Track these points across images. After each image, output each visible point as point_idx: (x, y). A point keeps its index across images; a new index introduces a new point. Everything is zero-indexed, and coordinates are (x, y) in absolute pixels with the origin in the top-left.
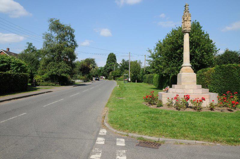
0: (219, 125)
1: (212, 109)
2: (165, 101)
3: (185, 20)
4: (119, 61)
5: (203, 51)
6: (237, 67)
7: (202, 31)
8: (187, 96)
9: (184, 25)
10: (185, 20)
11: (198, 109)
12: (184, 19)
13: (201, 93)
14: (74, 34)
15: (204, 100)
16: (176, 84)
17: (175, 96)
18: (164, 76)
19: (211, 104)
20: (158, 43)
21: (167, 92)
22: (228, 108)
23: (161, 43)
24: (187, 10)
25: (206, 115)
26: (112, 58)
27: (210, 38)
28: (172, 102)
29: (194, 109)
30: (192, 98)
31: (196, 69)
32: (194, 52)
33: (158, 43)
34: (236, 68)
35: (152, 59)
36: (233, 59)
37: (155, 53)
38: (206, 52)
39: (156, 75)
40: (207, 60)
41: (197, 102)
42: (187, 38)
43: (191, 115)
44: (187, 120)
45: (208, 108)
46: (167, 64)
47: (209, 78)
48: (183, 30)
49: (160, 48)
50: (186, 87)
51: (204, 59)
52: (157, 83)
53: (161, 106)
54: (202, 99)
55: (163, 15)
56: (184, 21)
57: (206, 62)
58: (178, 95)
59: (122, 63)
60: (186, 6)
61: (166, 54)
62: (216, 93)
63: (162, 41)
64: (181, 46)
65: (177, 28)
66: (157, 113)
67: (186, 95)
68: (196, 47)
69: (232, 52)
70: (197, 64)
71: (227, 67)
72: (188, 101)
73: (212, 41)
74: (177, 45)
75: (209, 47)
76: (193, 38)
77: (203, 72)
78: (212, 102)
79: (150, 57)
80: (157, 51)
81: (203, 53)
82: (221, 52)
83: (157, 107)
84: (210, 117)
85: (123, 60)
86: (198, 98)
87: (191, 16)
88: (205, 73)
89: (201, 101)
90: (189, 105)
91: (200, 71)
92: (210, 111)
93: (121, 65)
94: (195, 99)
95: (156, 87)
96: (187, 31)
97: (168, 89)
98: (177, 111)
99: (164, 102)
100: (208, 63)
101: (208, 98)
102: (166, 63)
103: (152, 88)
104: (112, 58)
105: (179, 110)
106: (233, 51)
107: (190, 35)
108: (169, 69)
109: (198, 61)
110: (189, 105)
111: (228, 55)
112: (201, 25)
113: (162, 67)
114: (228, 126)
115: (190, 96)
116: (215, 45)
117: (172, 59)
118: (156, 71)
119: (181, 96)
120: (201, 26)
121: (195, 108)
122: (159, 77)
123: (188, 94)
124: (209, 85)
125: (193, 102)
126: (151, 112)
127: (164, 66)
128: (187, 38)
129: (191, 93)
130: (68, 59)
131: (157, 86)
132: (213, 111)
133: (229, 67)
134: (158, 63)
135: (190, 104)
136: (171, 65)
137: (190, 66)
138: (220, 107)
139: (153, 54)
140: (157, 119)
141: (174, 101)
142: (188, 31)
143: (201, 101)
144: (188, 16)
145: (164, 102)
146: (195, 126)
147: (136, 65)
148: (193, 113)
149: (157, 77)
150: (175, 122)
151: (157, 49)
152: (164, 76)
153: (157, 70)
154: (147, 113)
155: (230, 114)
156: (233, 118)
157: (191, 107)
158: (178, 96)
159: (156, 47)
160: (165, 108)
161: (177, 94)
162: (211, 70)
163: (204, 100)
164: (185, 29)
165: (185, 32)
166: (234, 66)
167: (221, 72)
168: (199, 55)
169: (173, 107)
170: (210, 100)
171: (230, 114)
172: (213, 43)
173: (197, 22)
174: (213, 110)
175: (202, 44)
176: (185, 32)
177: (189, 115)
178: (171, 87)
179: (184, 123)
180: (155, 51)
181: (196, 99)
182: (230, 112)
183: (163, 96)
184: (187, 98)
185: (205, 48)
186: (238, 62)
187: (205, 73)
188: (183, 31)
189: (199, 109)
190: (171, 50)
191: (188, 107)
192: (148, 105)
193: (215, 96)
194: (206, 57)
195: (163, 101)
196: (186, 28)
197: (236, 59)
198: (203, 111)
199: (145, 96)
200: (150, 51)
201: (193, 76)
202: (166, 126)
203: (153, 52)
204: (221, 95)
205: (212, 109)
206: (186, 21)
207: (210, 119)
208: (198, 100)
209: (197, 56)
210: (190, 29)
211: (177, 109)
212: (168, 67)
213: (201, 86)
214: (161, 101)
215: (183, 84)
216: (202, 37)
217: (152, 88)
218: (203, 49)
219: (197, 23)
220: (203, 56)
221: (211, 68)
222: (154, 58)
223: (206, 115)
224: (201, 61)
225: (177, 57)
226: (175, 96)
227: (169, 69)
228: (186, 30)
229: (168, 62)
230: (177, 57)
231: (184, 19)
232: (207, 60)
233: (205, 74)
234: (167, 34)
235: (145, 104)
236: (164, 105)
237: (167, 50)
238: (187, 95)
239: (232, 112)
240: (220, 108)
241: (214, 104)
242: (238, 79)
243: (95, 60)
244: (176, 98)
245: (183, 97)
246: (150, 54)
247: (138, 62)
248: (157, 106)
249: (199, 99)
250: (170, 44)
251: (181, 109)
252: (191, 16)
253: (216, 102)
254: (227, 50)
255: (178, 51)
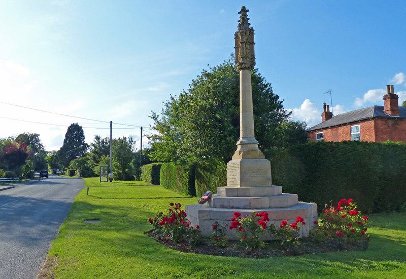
4: (89, 139)
14: (234, 37)
26: (75, 132)
27: (275, 92)
52: (150, 179)
59: (94, 143)
63: (177, 98)
65: (211, 69)
79: (154, 128)
85: (97, 138)
93: (93, 147)
99: (204, 230)
104: (75, 132)
145: (204, 230)
147: (123, 146)
151: (167, 113)
243: (39, 137)
247: (127, 140)
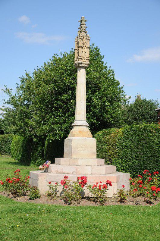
0: (136, 227)
1: (122, 201)
2: (43, 188)
3: (81, 45)
5: (105, 98)
6: (157, 130)
7: (104, 65)
8: (82, 178)
9: (78, 54)
10: (81, 45)
11: (101, 200)
12: (78, 43)
13: (104, 172)
15: (110, 185)
16: (62, 156)
17: (61, 178)
18: (35, 140)
19: (121, 193)
20: (25, 77)
21: (46, 171)
22: (146, 199)
23: (30, 78)
24: (83, 28)
25: (114, 211)
27: (117, 78)
28: (56, 189)
29: (94, 201)
30: (91, 182)
31: (94, 129)
32: (91, 99)
33: (25, 77)
34: (155, 130)
35: (11, 107)
36: (148, 113)
37: (17, 95)
38: (108, 101)
39: (17, 138)
40: (111, 115)
41: (100, 189)
42: (82, 77)
43: (91, 213)
44: (85, 220)
45: (116, 199)
46: (44, 118)
47: (114, 146)
48: (75, 62)
49: (29, 88)
50: (80, 162)
51: (107, 112)
53: (38, 197)
54: (107, 184)
55: (24, 19)
56: (79, 47)
57: (109, 118)
58: (67, 177)
60: (81, 21)
61: (42, 101)
62: (125, 172)
64: (71, 90)
65: (61, 54)
66: (32, 211)
67: (80, 176)
68: (94, 92)
69: (145, 101)
70: (95, 121)
71: (142, 128)
72: (85, 188)
73: (118, 83)
74: (62, 84)
75: (114, 93)
76: (90, 76)
77: (103, 135)
78: (121, 188)
79: (8, 103)
80: (21, 92)
81: (104, 102)
82: (132, 101)
83: (30, 199)
84: (121, 214)
86: (101, 182)
87: (89, 40)
88: (108, 137)
89: (105, 187)
90: (86, 195)
91: (100, 133)
92: (119, 203)
94: (95, 184)
95: (17, 161)
96: (83, 65)
97: (48, 166)
98: (67, 205)
100: (112, 120)
101: (115, 181)
102: (42, 116)
103: (9, 163)
105: (69, 204)
106: (148, 99)
107: (87, 73)
108: (46, 127)
109: (97, 116)
110: (86, 195)
111: (141, 107)
112: (102, 53)
113: (33, 123)
114: (149, 229)
115: (87, 179)
116: (123, 89)
117: (52, 111)
118: (20, 131)
119: (73, 179)
120: (102, 55)
121: (95, 200)
122: (24, 140)
123: (85, 176)
124: (113, 159)
125: (92, 188)
126: (23, 210)
127: (38, 122)
128: (82, 77)
129: (88, 173)
130: (34, 159)
131: (19, 158)
132: (123, 204)
133: (145, 129)
134: (24, 115)
135: (87, 192)
136: (50, 121)
137: (87, 126)
138: (132, 196)
139: (13, 98)
140: (35, 222)
141: (60, 188)
142: (85, 65)
143: (105, 187)
144: (84, 40)
146: (102, 231)
148: (94, 208)
149: (19, 141)
150: (66, 226)
152: (35, 140)
153: (21, 128)
154: (13, 211)
155: (150, 208)
156: (154, 214)
157: (88, 198)
158: (68, 179)
159: (20, 83)
160: (43, 201)
161: (64, 175)
162: (117, 132)
163: (110, 185)
164: (80, 61)
165: (79, 67)
166: (151, 127)
167: (132, 136)
168: (98, 105)
169: (58, 199)
170: (118, 185)
171: (150, 208)
172: (120, 86)
173: (95, 47)
174: (124, 202)
175: (104, 85)
176: (79, 67)
177: (87, 211)
178: (53, 162)
179: (84, 227)
180: (18, 93)
181: (97, 183)
182: (148, 205)
183: (40, 178)
184: (83, 181)
185: (108, 94)
186: (155, 118)
187: (108, 137)
188: (76, 64)
189: (102, 201)
190: (51, 92)
191: (83, 198)
192: (11, 196)
193: (125, 179)
194: (109, 109)
195: (39, 188)
196: (81, 59)
197: (152, 113)
198: (109, 204)
199: (5, 180)
200: (8, 92)
201: (92, 142)
202: (54, 233)
203: (14, 92)
204: (133, 176)
205: (122, 201)
206: (82, 47)
207: (122, 217)
208: (100, 186)
209: (95, 107)
210: (88, 62)
211: (66, 202)
212: (44, 124)
213: (103, 160)
214: (36, 189)
215: (74, 156)
216: (103, 75)
217: (9, 163)
218: (106, 96)
219: (96, 49)
220: (104, 108)
221: (116, 130)
222: (15, 105)
223: (114, 211)
224: (101, 115)
225: (61, 107)
226: (63, 178)
227: (46, 127)
228: (81, 63)
229: (46, 115)
230: (61, 107)
231: (78, 43)
232: (111, 115)
233: (108, 140)
234: (45, 64)
235: (6, 195)
236: (42, 196)
237: (44, 93)
238: (82, 176)
239: (152, 205)
240: (133, 199)
241: (125, 193)
242: (158, 149)
244: (64, 183)
245: (75, 180)
246: (8, 98)
248: (28, 198)
249: (102, 184)
250: (49, 82)
251: (72, 202)
252: (89, 40)
253: (127, 189)
254: (138, 97)
255: (64, 97)
